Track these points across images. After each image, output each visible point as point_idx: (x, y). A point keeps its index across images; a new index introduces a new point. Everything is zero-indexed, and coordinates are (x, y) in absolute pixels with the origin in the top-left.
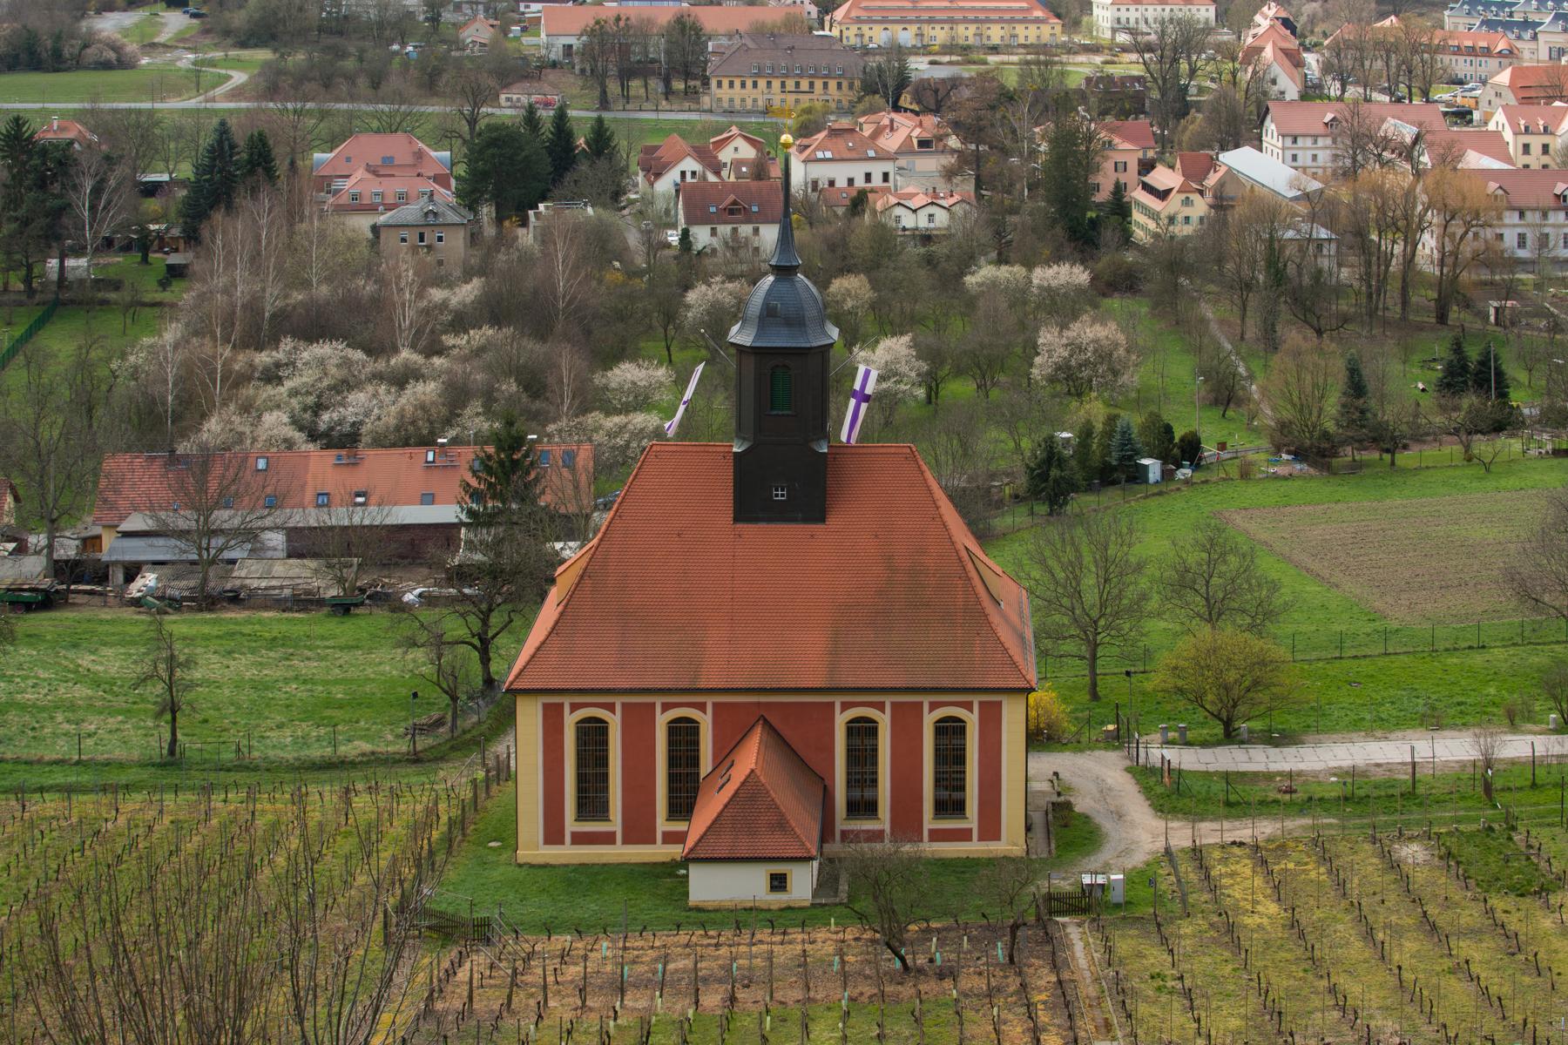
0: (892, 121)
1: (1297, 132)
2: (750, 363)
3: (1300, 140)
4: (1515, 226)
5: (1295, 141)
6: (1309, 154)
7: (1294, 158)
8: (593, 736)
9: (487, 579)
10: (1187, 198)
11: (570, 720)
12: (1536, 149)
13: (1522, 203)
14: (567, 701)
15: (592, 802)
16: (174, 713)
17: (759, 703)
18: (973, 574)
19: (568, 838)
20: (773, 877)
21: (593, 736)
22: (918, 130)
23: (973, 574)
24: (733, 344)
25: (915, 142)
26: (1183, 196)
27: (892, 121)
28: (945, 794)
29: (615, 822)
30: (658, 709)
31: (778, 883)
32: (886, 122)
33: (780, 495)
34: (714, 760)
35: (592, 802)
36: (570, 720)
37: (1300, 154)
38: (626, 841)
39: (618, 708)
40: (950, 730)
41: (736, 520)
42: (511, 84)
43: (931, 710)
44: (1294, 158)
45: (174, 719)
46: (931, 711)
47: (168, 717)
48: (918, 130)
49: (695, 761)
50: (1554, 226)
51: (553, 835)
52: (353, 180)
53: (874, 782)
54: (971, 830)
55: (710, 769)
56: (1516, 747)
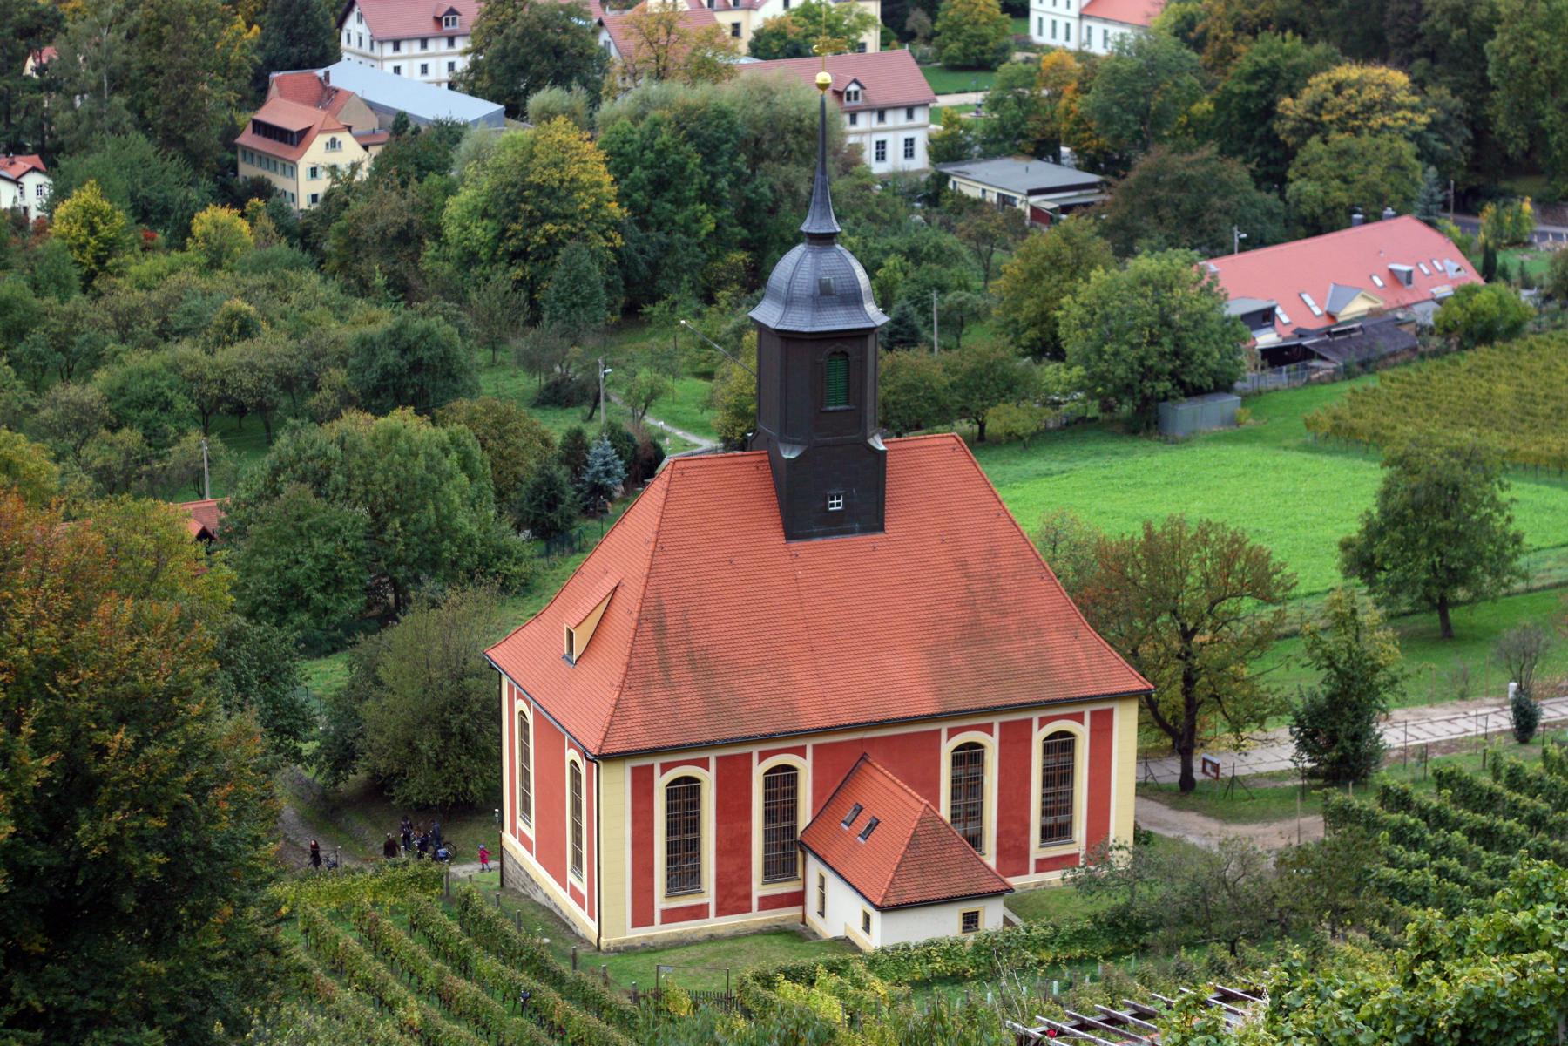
1: (397, 34)
2: (775, 346)
8: (684, 795)
10: (333, 140)
11: (661, 783)
13: (880, 101)
14: (657, 763)
15: (683, 873)
17: (861, 741)
19: (755, 903)
21: (684, 795)
26: (327, 138)
29: (709, 893)
30: (657, 770)
31: (970, 921)
33: (836, 505)
34: (815, 804)
35: (683, 873)
36: (661, 783)
37: (431, 63)
38: (721, 911)
39: (713, 764)
40: (1060, 745)
43: (663, 772)
46: (1041, 727)
49: (791, 812)
51: (642, 916)
54: (707, 905)
55: (809, 821)
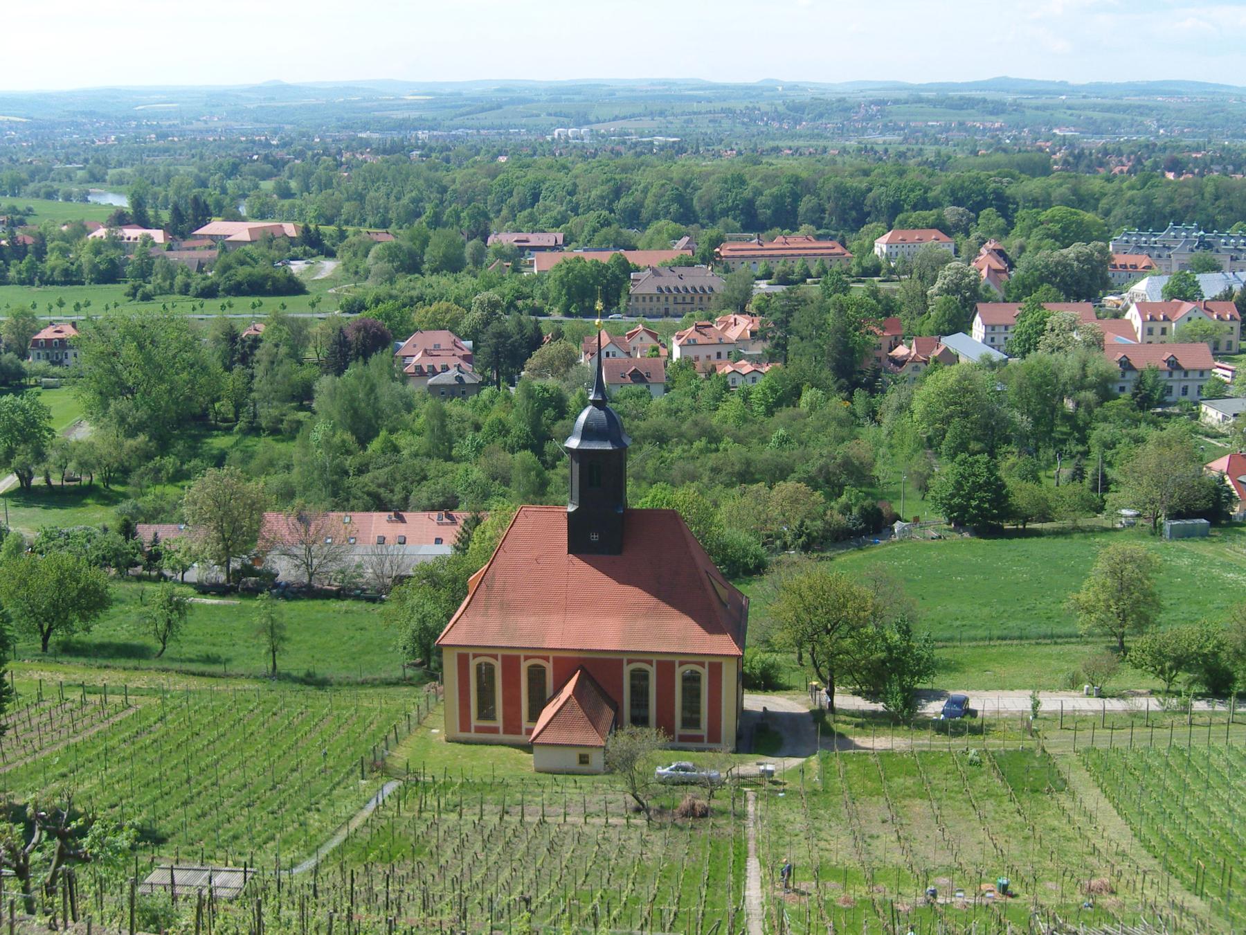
0: (735, 320)
1: (994, 322)
3: (997, 328)
4: (1197, 380)
5: (993, 330)
6: (1003, 336)
7: (993, 340)
9: (639, 766)
12: (1157, 331)
16: (274, 652)
18: (710, 588)
20: (587, 762)
22: (751, 325)
23: (710, 588)
24: (757, 481)
25: (748, 332)
27: (735, 320)
28: (688, 715)
32: (732, 320)
37: (996, 337)
41: (569, 553)
42: (933, 103)
44: (993, 340)
45: (274, 656)
47: (271, 654)
48: (751, 325)
50: (1193, 380)
52: (415, 359)
53: (647, 706)
56: (1051, 703)
